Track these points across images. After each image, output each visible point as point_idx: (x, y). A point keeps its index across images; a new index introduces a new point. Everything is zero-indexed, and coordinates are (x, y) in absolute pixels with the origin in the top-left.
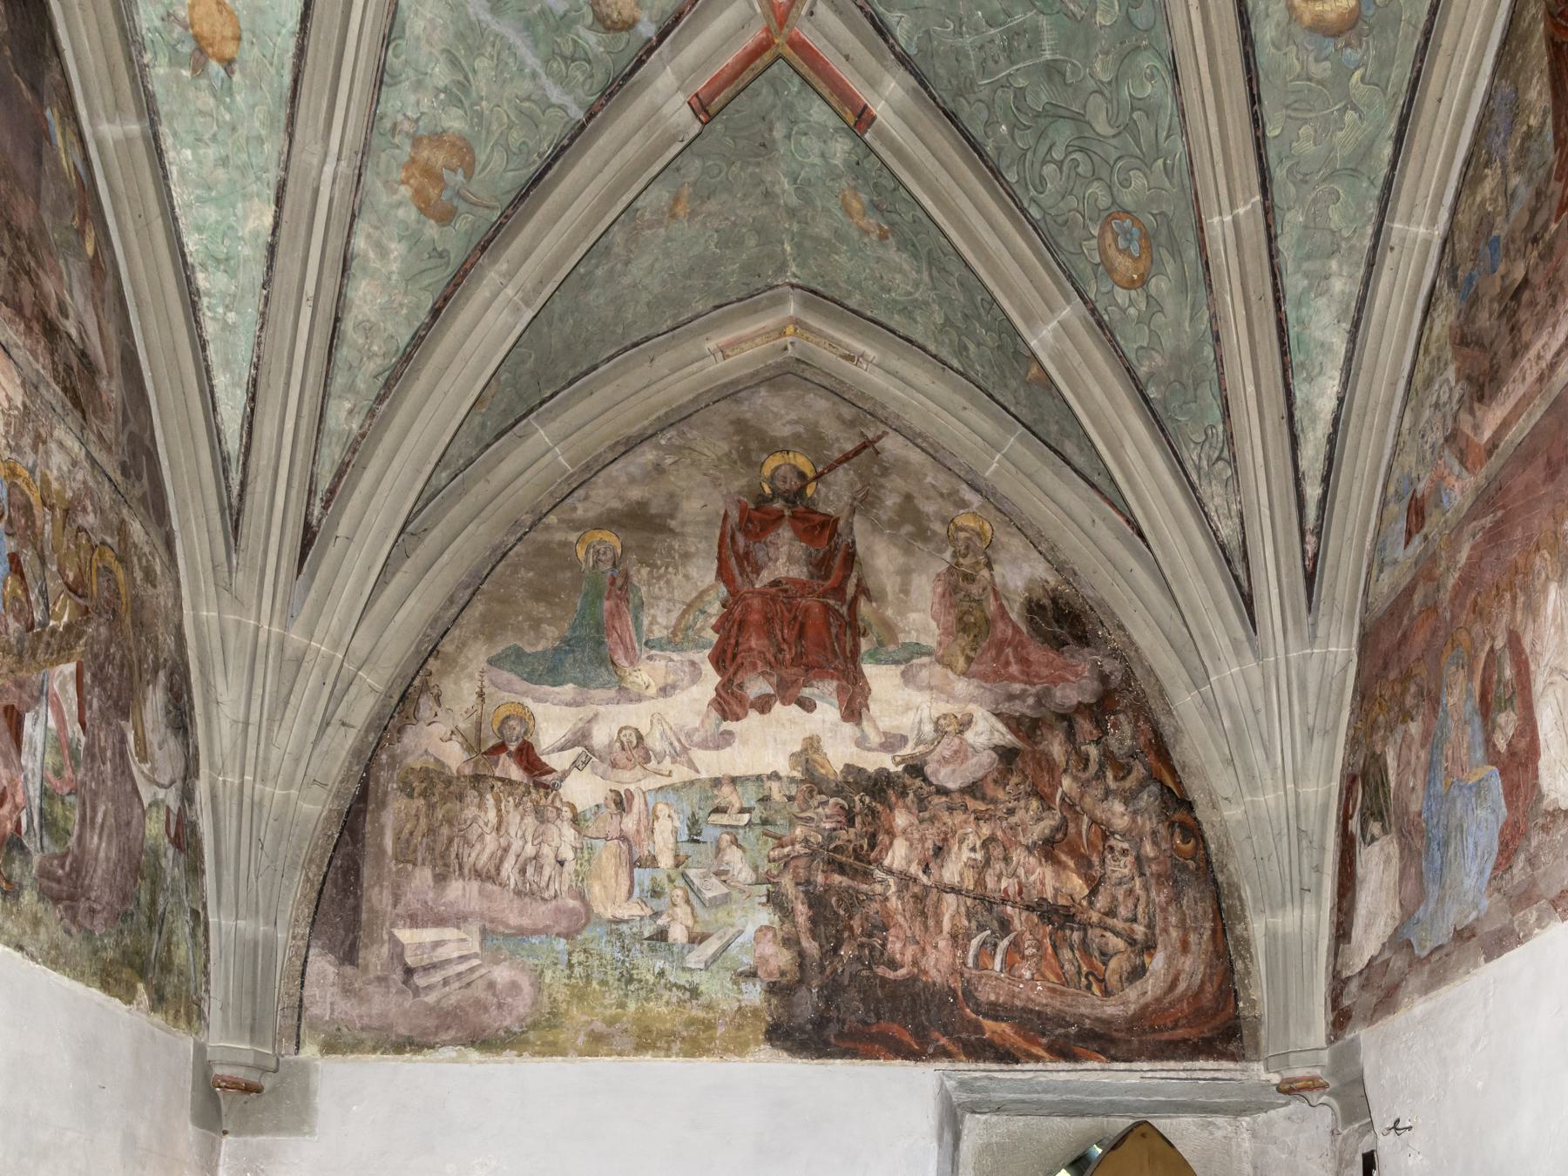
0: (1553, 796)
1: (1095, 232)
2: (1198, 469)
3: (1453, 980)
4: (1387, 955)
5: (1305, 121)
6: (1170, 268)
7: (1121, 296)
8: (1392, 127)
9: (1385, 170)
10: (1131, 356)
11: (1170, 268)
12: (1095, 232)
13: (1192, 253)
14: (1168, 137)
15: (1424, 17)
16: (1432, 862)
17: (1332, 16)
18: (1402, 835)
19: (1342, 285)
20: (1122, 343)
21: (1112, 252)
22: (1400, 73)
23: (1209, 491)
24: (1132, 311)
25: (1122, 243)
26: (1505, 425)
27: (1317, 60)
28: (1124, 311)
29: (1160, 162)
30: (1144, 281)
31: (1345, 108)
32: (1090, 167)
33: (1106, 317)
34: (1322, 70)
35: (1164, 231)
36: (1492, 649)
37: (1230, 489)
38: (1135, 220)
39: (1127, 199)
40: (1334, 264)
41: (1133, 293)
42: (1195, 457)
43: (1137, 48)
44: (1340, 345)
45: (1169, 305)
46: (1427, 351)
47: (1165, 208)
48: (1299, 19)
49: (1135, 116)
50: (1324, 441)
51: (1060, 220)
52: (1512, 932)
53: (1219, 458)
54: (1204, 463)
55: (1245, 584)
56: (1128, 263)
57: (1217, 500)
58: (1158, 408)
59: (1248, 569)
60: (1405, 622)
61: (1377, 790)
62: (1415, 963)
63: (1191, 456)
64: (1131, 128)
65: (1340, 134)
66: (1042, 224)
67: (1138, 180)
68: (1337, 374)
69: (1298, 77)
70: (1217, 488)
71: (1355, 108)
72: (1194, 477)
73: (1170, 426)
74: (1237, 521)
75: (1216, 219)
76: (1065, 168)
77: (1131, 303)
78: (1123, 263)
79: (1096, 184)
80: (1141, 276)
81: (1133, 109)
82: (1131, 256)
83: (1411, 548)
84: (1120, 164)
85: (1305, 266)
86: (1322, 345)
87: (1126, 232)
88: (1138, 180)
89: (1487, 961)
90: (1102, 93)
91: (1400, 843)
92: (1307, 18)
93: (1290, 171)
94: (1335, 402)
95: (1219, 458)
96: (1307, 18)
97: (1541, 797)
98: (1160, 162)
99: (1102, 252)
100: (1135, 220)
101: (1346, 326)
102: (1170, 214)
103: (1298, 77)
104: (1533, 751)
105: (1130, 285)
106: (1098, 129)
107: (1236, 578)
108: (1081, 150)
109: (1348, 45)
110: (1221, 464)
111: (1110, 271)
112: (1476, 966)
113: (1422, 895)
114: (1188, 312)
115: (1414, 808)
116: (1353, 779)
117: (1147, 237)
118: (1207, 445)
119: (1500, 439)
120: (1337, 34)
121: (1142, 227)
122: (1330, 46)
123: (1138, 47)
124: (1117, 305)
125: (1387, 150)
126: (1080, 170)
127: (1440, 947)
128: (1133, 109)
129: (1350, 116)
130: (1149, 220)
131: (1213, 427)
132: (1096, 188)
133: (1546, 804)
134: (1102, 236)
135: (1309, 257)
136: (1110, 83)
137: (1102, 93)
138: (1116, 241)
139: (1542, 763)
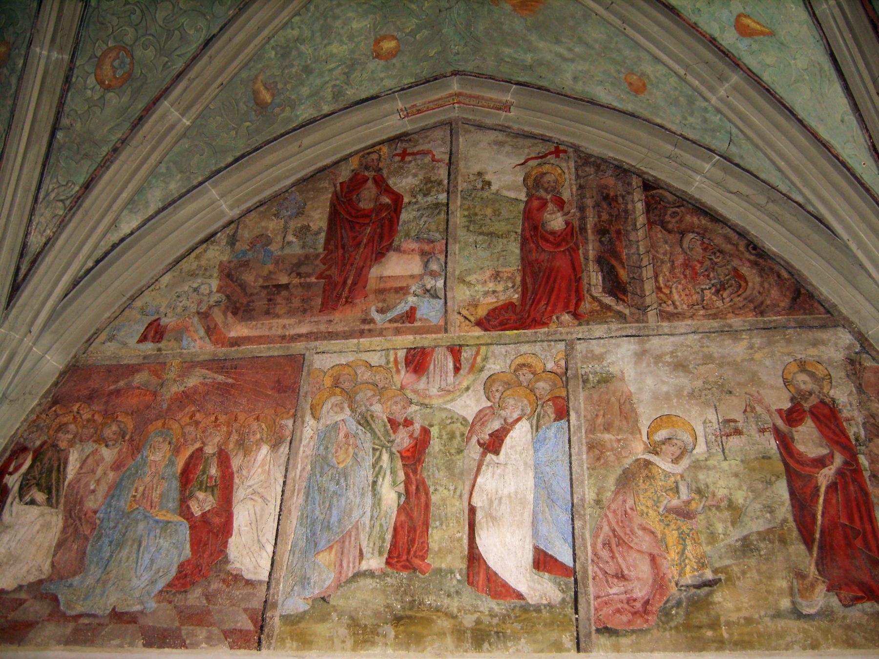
0: (238, 565)
1: (110, 44)
2: (47, 194)
3: (102, 645)
4: (23, 595)
5: (222, 116)
6: (125, 99)
7: (91, 81)
8: (238, 154)
9: (223, 165)
10: (66, 109)
11: (125, 99)
12: (110, 44)
13: (140, 105)
14: (179, 56)
15: (278, 133)
16: (100, 550)
17: (262, 97)
18: (69, 515)
19: (175, 187)
20: (69, 98)
21: (108, 61)
22: (259, 139)
23: (43, 210)
24: (89, 92)
25: (116, 63)
26: (248, 340)
27: (245, 103)
28: (86, 88)
29: (167, 59)
30: (108, 88)
31: (234, 129)
32: (138, 21)
33: (74, 80)
34: (243, 107)
35: (139, 84)
36: (201, 449)
37: (54, 221)
38: (132, 63)
39: (138, 53)
40: (179, 176)
41: (98, 87)
42: (51, 187)
43: (204, 15)
44: (151, 212)
45: (108, 111)
46: (197, 257)
47: (149, 75)
48: (254, 83)
49: (176, 32)
50: (111, 244)
51: (101, 19)
52: (179, 637)
53: (62, 201)
54: (53, 195)
55: (21, 277)
56: (110, 74)
57: (43, 220)
58: (55, 145)
59: (30, 270)
60: (121, 384)
61: (50, 471)
62: (57, 615)
63: (49, 184)
64: (170, 34)
65: (225, 135)
66: (91, 10)
67: (150, 53)
68: (139, 221)
69: (235, 100)
70: (48, 213)
71: (236, 133)
72: (41, 196)
73: (52, 160)
74: (44, 240)
75: (38, 50)
76: (128, 7)
77: (92, 89)
78: (107, 69)
79: (132, 30)
80: (109, 86)
81: (178, 29)
82: (114, 73)
83: (142, 346)
84: (151, 37)
85: (171, 164)
86: (147, 202)
87: (123, 62)
88: (150, 53)
89: (144, 645)
90: (174, 7)
91: (66, 521)
92: (256, 86)
93: (201, 125)
94: (129, 231)
95: (62, 201)
96: (256, 86)
97: (227, 561)
98: (167, 59)
99: (105, 54)
100: (132, 63)
101: (160, 205)
102: (148, 81)
103: (235, 100)
104: (226, 529)
105: (101, 83)
106: (157, 15)
107: (18, 269)
108: (142, 11)
109: (255, 111)
110: (60, 204)
111: (99, 66)
112: (131, 644)
113: (80, 566)
114: (112, 124)
115: (90, 504)
116: (24, 449)
117: (129, 76)
118: (63, 188)
119: (243, 344)
120: (257, 104)
121: (132, 69)
122: (252, 104)
123: (204, 15)
124: (85, 81)
125: (230, 159)
126: (133, 16)
127: (94, 616)
128: (178, 29)
129: (233, 133)
130: (137, 72)
131: (73, 183)
132: (131, 31)
133: (229, 567)
134: (111, 49)
135: (175, 163)
136: (181, 9)
137: (174, 7)
138: (114, 60)
139: (232, 541)
